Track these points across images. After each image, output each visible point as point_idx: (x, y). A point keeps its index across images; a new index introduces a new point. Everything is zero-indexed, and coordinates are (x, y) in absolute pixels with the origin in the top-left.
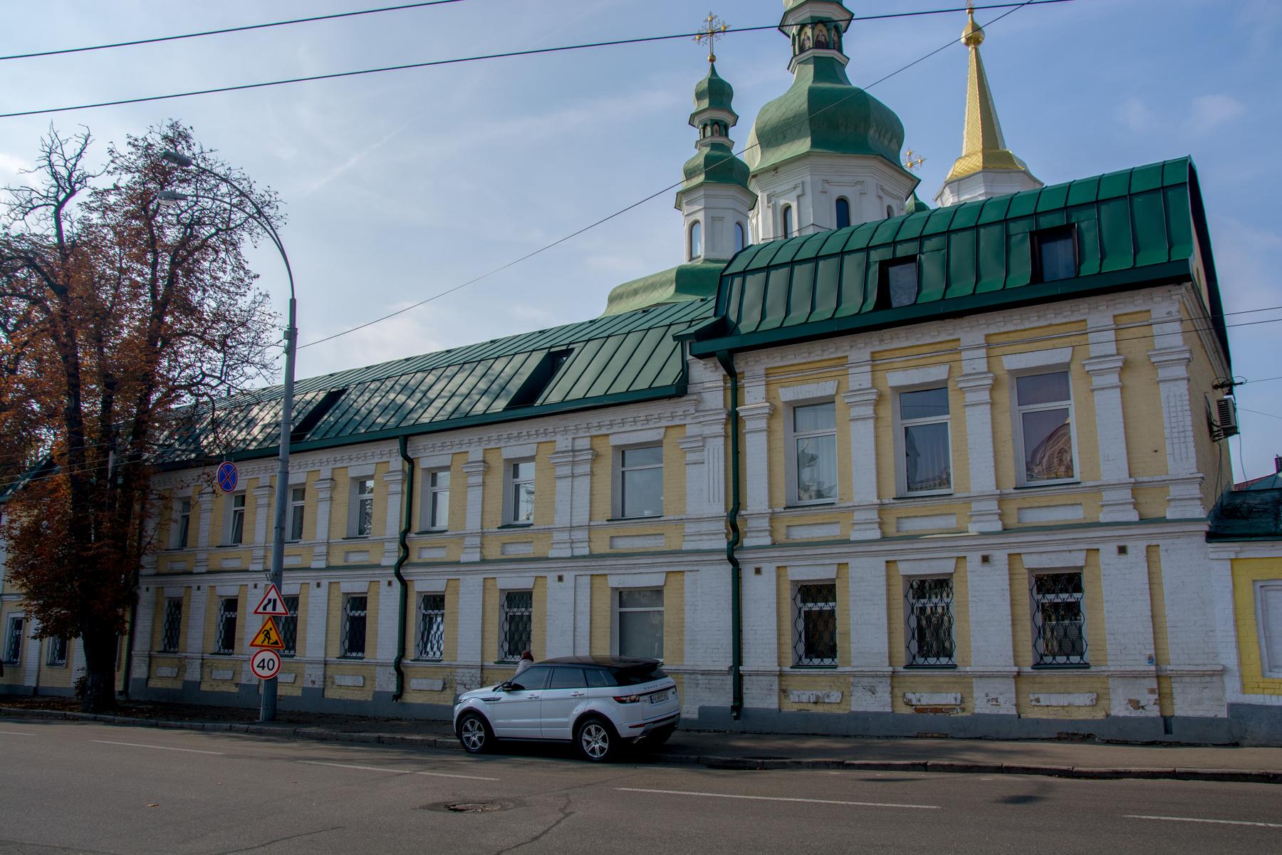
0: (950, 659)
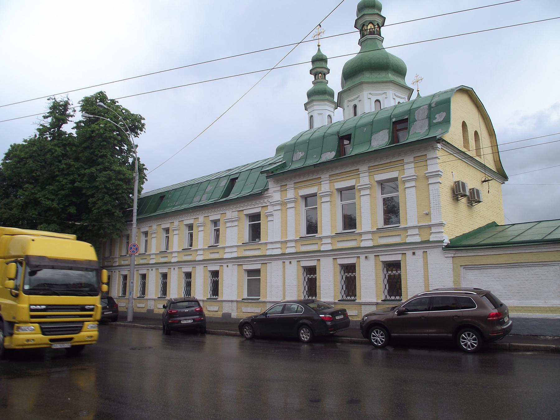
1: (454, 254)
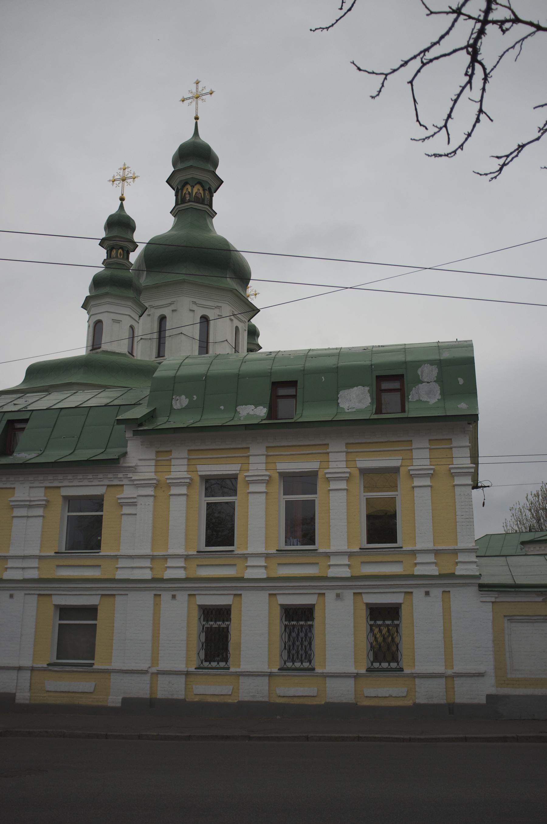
0: (226, 663)
1: (496, 598)
